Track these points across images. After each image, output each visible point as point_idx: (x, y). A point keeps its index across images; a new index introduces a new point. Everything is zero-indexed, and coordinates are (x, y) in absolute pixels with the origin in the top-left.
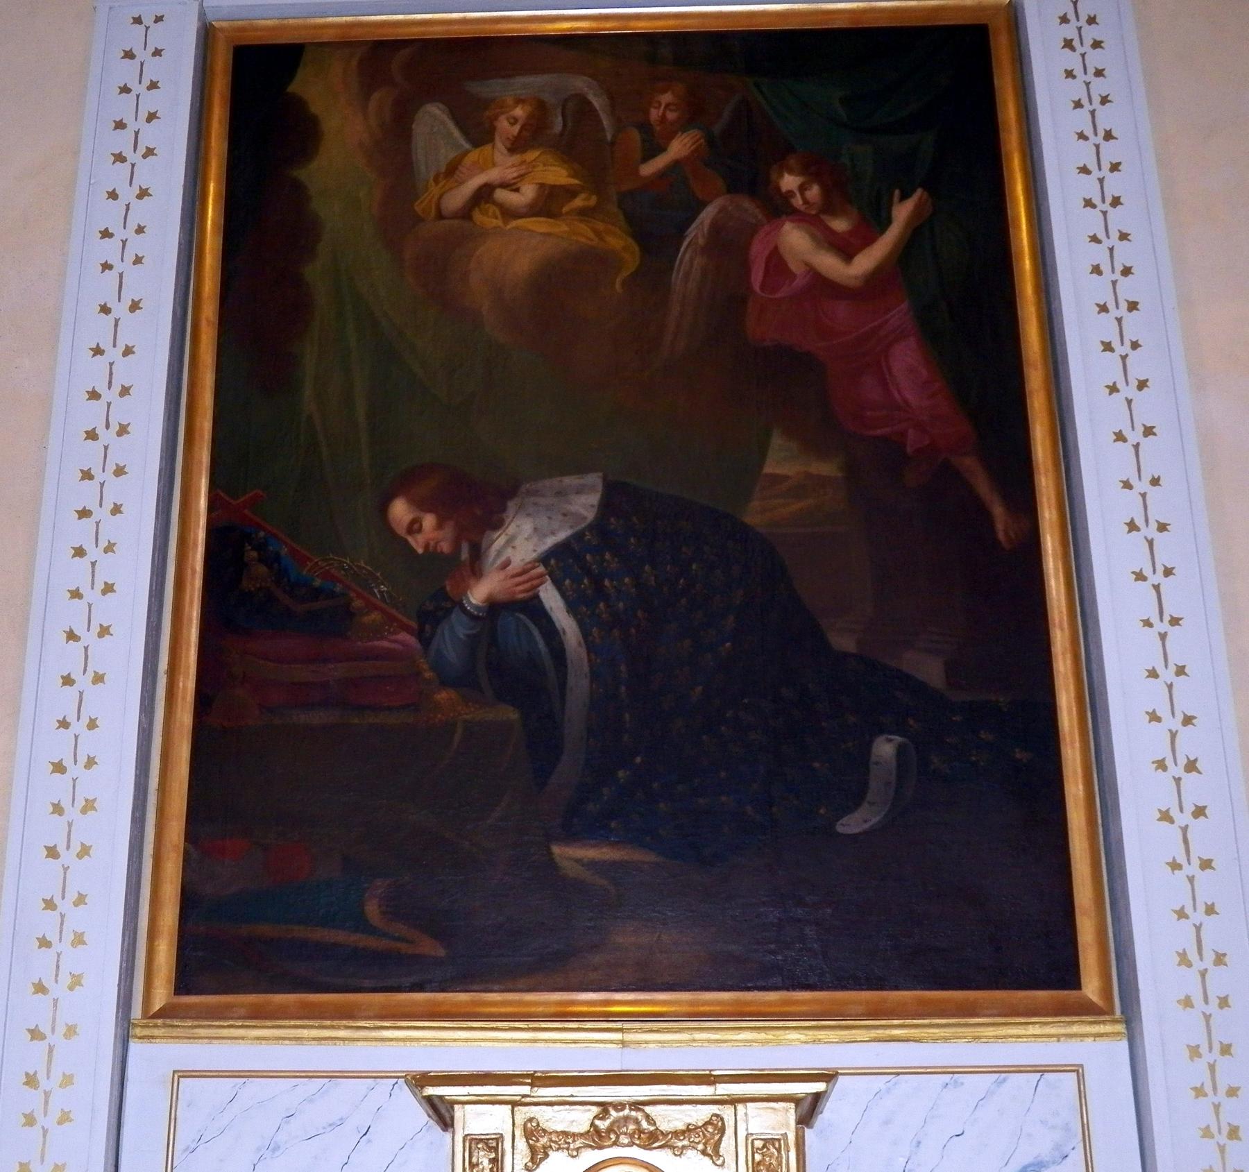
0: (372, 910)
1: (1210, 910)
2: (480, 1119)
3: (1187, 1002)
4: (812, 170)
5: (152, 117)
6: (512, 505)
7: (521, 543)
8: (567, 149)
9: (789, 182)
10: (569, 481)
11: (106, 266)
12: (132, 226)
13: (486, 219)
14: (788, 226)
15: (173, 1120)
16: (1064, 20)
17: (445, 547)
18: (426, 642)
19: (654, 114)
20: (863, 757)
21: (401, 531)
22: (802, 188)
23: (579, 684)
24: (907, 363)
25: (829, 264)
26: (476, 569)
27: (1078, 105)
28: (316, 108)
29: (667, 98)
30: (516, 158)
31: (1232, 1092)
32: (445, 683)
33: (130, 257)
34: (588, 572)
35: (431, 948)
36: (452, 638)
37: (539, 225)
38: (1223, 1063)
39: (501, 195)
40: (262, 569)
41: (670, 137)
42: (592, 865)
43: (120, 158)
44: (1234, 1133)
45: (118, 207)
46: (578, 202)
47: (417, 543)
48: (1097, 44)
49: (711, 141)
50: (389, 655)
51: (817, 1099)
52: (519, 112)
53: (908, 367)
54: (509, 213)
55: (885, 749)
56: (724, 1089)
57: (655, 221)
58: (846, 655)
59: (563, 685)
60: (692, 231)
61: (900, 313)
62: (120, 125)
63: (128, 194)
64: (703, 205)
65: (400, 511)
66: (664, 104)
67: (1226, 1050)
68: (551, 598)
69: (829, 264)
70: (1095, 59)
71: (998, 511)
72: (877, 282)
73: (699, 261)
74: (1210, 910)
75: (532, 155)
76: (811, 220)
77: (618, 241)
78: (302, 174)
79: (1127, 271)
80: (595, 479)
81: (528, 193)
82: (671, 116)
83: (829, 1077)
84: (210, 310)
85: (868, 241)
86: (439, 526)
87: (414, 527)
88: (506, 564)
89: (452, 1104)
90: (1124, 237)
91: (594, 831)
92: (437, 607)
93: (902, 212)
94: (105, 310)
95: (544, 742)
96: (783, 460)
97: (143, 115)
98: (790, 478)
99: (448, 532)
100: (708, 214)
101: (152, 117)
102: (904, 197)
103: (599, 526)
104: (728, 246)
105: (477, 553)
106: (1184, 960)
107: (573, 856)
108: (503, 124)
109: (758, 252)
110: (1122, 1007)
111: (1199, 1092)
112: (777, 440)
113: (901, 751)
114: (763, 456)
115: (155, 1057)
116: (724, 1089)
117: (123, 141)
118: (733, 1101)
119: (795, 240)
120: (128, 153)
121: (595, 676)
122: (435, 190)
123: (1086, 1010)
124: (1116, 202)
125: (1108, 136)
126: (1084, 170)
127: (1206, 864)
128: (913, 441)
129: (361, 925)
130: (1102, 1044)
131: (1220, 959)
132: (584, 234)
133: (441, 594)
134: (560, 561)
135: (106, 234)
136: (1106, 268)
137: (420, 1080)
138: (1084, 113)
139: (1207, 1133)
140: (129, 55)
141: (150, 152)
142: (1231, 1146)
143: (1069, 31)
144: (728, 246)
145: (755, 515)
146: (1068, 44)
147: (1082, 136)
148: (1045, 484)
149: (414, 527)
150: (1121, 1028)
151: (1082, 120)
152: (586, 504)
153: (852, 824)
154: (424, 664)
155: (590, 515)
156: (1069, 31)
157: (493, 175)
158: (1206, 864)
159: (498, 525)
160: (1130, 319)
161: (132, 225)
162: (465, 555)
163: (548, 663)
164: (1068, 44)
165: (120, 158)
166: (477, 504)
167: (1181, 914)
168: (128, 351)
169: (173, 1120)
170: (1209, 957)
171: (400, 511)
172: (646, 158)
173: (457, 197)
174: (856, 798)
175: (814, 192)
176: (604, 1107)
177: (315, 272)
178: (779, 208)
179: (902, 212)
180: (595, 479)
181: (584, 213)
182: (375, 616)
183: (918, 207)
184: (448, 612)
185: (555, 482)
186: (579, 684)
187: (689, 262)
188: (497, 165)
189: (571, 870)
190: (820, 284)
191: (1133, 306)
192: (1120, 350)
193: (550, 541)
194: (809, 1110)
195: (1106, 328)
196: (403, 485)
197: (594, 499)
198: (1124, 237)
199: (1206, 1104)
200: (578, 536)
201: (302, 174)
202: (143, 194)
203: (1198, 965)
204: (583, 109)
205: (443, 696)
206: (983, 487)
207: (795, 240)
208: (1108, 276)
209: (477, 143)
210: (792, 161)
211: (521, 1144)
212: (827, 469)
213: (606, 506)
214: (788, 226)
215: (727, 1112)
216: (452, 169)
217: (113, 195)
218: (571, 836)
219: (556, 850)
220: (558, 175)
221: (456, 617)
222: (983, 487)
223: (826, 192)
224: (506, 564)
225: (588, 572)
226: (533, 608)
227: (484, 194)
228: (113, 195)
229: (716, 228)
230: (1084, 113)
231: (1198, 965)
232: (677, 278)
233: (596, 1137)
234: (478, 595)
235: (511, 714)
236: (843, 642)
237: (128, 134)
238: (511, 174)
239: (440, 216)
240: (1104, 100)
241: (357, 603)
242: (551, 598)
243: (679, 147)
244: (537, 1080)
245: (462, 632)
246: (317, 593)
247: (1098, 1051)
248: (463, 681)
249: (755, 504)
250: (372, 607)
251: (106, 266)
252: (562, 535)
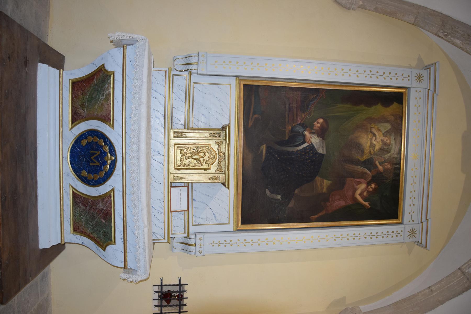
0: (256, 116)
1: (252, 245)
2: (222, 133)
3: (238, 240)
4: (375, 189)
5: (391, 79)
6: (321, 139)
7: (315, 140)
8: (381, 149)
9: (373, 186)
10: (325, 148)
11: (365, 71)
12: (372, 76)
13: (370, 136)
14: (365, 185)
15: (223, 84)
16: (397, 232)
17: (314, 128)
18: (299, 124)
19: (386, 164)
20: (277, 193)
21: (317, 121)
22: (372, 188)
23: (291, 149)
24: (342, 203)
25: (359, 192)
26: (311, 133)
27: (382, 233)
28: (391, 107)
29: (389, 166)
30: (380, 140)
31: (225, 246)
32: (292, 128)
33: (366, 75)
34: (309, 151)
35: (250, 124)
36: (300, 129)
37: (368, 144)
38: (229, 245)
39: (374, 138)
40: (312, 97)
41: (383, 166)
42: (262, 151)
43: (384, 73)
44: (219, 245)
45: (375, 73)
46: (372, 151)
47: (315, 123)
48: (392, 237)
49: (381, 173)
50: (297, 118)
51: (225, 186)
52: (388, 141)
53: (339, 203)
54: (371, 139)
55: (279, 197)
56: (227, 172)
57: (369, 163)
58: (294, 192)
59: (291, 147)
60: (366, 169)
61: (350, 202)
62: (390, 73)
63: (377, 75)
64: (370, 171)
65: (321, 121)
66: (388, 166)
67: (231, 245)
68: (305, 145)
69: (359, 192)
70: (390, 236)
71: (316, 216)
72: (355, 199)
73: (361, 170)
74: (252, 245)
75: (381, 143)
76: (366, 189)
77: (365, 157)
78: (379, 104)
79: (354, 239)
80: (325, 152)
81: (375, 143)
82: (386, 167)
83: (228, 188)
84: (357, 89)
85: (362, 198)
86: (318, 127)
87: (318, 123)
88: (311, 138)
89: (225, 130)
90: (360, 239)
91: (268, 151)
92: (305, 126)
93: (367, 204)
94: (357, 71)
95: (283, 143)
96: (326, 183)
97: (391, 77)
98: (323, 184)
99: (317, 128)
100: (369, 172)
101: (391, 79)
102: (369, 204)
103: (317, 153)
104: (363, 176)
105: (313, 133)
106: (245, 240)
107: (264, 148)
108: (387, 138)
109: (362, 180)
110: (237, 230)
111: (225, 241)
112: (330, 182)
113: (279, 199)
114: (327, 180)
115: (234, 82)
116: (227, 172)
117: (387, 74)
118: (225, 173)
119: (363, 186)
120: (385, 75)
121: (292, 152)
122: (376, 127)
123: (237, 225)
124: (365, 238)
125: (377, 237)
126: (371, 233)
127: (259, 244)
128: (328, 204)
129: (254, 114)
130: (233, 227)
131: (245, 245)
132: (367, 151)
133: (307, 127)
134: (311, 147)
135: (371, 71)
136: (355, 236)
137: (229, 125)
138: (381, 234)
139: (219, 242)
140: (403, 75)
141: (385, 78)
142: (217, 245)
143: (395, 232)
144: (363, 176)
145: (318, 179)
146: (393, 232)
147: (377, 233)
148: (320, 224)
149: (318, 123)
150: (235, 230)
151: (357, 235)
152: (321, 151)
153: (267, 192)
154: (295, 124)
155: (319, 152)
156: (395, 232)
157: (378, 136)
158: (259, 244)
159: (318, 136)
160: (346, 239)
161: (372, 76)
162: (313, 131)
163: (295, 144)
164: (393, 232)
165: (384, 73)
166: (322, 133)
167: (252, 240)
168: (350, 75)
169: (223, 84)
170: (245, 244)
171: (321, 121)
172: (379, 162)
173: (374, 131)
174: (272, 192)
175: (371, 190)
176: (224, 154)
177: (362, 106)
178: (369, 184)
179: (367, 204)
180: (325, 152)
181: (370, 151)
182: (303, 116)
183: (368, 207)
184: (304, 128)
185: (325, 146)
186: (291, 149)
187: (361, 169)
188: (380, 137)
189: (262, 147)
190: (355, 190)
191: (348, 239)
192: (341, 237)
193: (315, 145)
194: (224, 184)
195: (368, 234)
196: (325, 121)
197: (322, 152)
198: (360, 239)
199: (224, 242)
200: (315, 150)
201: (379, 104)
202: (377, 77)
203: (244, 242)
204: (388, 151)
205: (290, 127)
206: (320, 214)
207: (363, 186)
208: (353, 236)
209: (383, 134)
210: (377, 186)
211: (219, 141)
212: (325, 190)
213: (320, 154)
214: (365, 185)
215: (224, 172)
216: (379, 130)
217: (377, 72)
218: (268, 147)
219: (265, 145)
220: (377, 147)
221: (303, 129)
222: (320, 214)
223: (371, 191)
224: (311, 138)
225: (309, 151)
226: (304, 142)
227: (374, 135)
228: (377, 72)
229: (366, 173)
230: (381, 234)
231: (244, 242)
232: (358, 167)
233: (220, 152)
234: (306, 133)
235: (287, 139)
236: (296, 191)
237: (388, 75)
238: (378, 140)
239: (371, 128)
240: (383, 237)
241: (306, 113)
242: (305, 145)
243: (380, 168)
244: (229, 144)
245: (300, 130)
246: (308, 106)
247: (231, 227)
248: (292, 131)
249: (319, 178)
250: (305, 115)
251: (365, 71)
252: (316, 147)
